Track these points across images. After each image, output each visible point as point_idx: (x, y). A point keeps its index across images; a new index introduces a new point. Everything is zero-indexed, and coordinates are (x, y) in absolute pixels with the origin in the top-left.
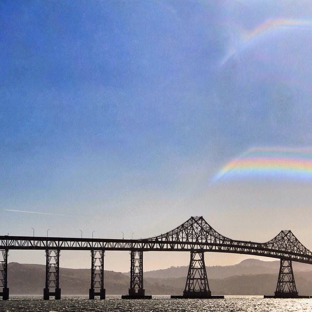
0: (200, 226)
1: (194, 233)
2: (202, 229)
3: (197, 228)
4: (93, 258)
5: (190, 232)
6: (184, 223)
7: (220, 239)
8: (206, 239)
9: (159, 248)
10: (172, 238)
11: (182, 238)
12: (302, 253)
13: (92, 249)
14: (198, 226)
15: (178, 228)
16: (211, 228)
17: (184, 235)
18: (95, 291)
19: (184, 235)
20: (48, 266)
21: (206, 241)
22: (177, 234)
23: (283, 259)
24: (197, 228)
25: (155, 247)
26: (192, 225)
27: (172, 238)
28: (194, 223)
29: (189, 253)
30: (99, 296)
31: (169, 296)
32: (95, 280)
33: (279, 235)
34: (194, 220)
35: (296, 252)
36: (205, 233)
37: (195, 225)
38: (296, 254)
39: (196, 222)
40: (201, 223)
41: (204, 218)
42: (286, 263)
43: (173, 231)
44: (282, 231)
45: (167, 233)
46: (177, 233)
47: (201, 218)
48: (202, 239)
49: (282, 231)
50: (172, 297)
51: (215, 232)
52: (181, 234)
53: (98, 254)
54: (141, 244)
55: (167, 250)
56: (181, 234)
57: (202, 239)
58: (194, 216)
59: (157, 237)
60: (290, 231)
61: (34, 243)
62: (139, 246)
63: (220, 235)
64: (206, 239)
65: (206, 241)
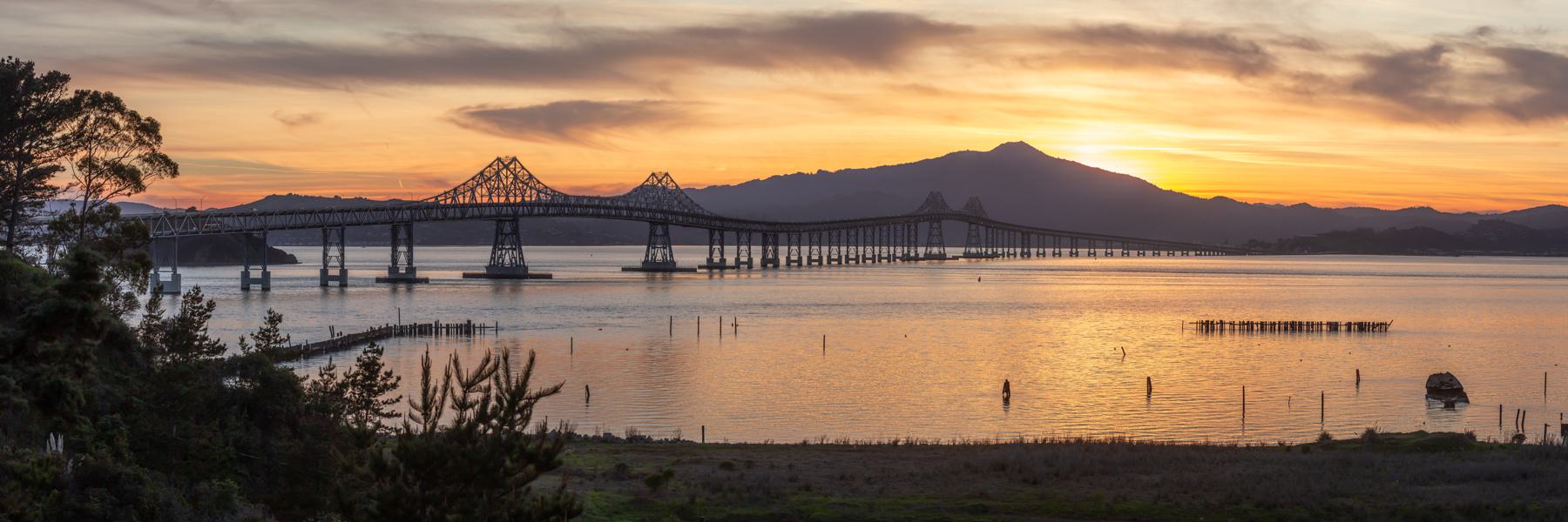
0: (512, 173)
1: (501, 185)
2: (516, 177)
3: (507, 177)
5: (496, 186)
6: (484, 170)
7: (546, 193)
9: (511, 213)
11: (482, 197)
12: (686, 211)
14: (509, 173)
15: (473, 179)
16: (531, 177)
17: (484, 192)
19: (485, 191)
21: (523, 199)
22: (473, 190)
23: (971, 223)
24: (507, 177)
25: (434, 215)
26: (498, 173)
30: (260, 285)
31: (458, 274)
32: (867, 234)
33: (490, 166)
34: (502, 163)
35: (676, 209)
36: (520, 185)
37: (504, 171)
39: (506, 167)
40: (515, 170)
41: (518, 158)
42: (973, 227)
44: (653, 174)
45: (455, 189)
46: (472, 189)
48: (499, 196)
49: (653, 174)
50: (465, 276)
51: (539, 182)
54: (566, 212)
56: (479, 191)
57: (515, 195)
58: (502, 156)
60: (667, 174)
61: (351, 218)
63: (546, 187)
64: (523, 196)
65: (523, 199)
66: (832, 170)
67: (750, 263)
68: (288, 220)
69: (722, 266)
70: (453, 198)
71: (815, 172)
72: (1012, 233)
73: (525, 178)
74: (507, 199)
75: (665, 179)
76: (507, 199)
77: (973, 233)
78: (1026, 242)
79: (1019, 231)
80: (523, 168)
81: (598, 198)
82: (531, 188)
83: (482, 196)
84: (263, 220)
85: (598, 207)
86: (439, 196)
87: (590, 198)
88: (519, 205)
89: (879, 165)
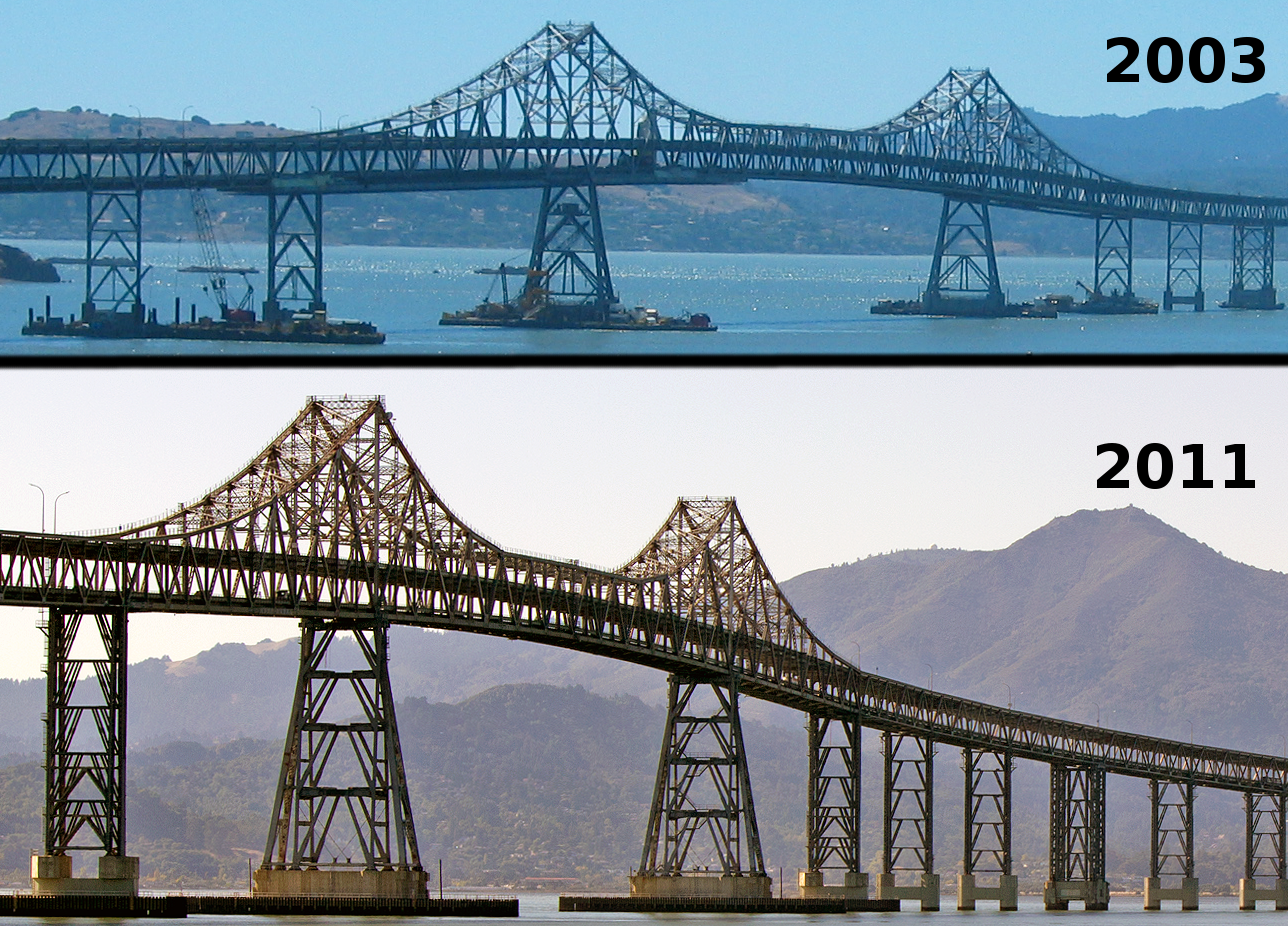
0: (583, 63)
3: (570, 75)
14: (575, 62)
40: (591, 56)
42: (704, 700)
51: (653, 89)
67: (1198, 301)
68: (336, 161)
70: (431, 125)
72: (989, 761)
73: (618, 77)
74: (571, 128)
75: (981, 87)
76: (571, 128)
77: (705, 792)
79: (1030, 752)
80: (612, 52)
81: (808, 130)
84: (358, 159)
85: (807, 152)
86: (395, 118)
87: (788, 130)
88: (559, 144)
89: (162, 117)
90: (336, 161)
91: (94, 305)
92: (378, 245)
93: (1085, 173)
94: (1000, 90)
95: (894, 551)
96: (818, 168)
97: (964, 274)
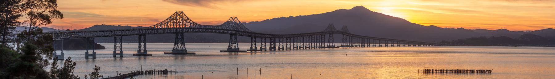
0: (181, 17)
1: (177, 21)
2: (183, 19)
3: (179, 19)
4: (300, 39)
5: (176, 22)
8: (185, 25)
10: (164, 26)
13: (386, 40)
14: (180, 17)
15: (167, 19)
16: (188, 18)
18: (301, 47)
19: (172, 23)
20: (256, 42)
21: (185, 26)
22: (167, 23)
24: (179, 19)
26: (176, 17)
27: (164, 26)
28: (178, 16)
29: (229, 36)
31: (162, 53)
33: (173, 15)
34: (178, 13)
35: (239, 30)
36: (184, 21)
38: (239, 31)
39: (179, 15)
40: (182, 16)
41: (183, 12)
43: (164, 21)
45: (161, 23)
46: (167, 23)
47: (182, 12)
48: (177, 25)
50: (165, 53)
51: (191, 20)
52: (170, 23)
53: (369, 40)
55: (191, 32)
57: (182, 25)
59: (154, 26)
62: (381, 39)
63: (193, 22)
64: (185, 25)
65: (185, 26)
66: (295, 16)
67: (265, 49)
68: (109, 33)
69: (256, 50)
70: (160, 26)
71: (288, 17)
74: (180, 26)
75: (235, 19)
76: (180, 26)
78: (363, 41)
80: (185, 15)
81: (212, 26)
82: (188, 22)
83: (170, 25)
86: (155, 25)
90: (115, 33)
91: (56, 53)
92: (489, 30)
93: (250, 31)
94: (238, 20)
95: (78, 77)
96: (200, 31)
97: (126, 49)
